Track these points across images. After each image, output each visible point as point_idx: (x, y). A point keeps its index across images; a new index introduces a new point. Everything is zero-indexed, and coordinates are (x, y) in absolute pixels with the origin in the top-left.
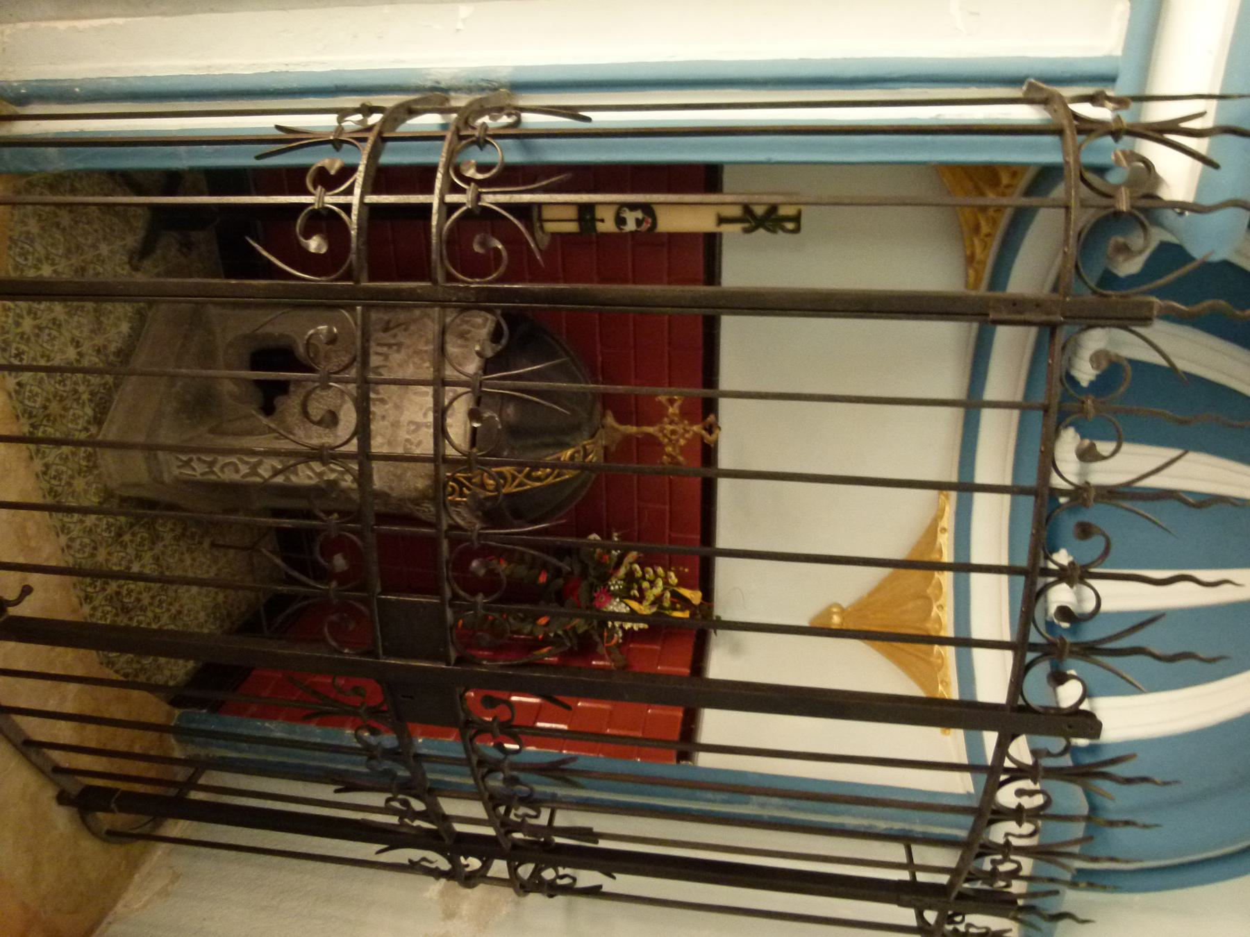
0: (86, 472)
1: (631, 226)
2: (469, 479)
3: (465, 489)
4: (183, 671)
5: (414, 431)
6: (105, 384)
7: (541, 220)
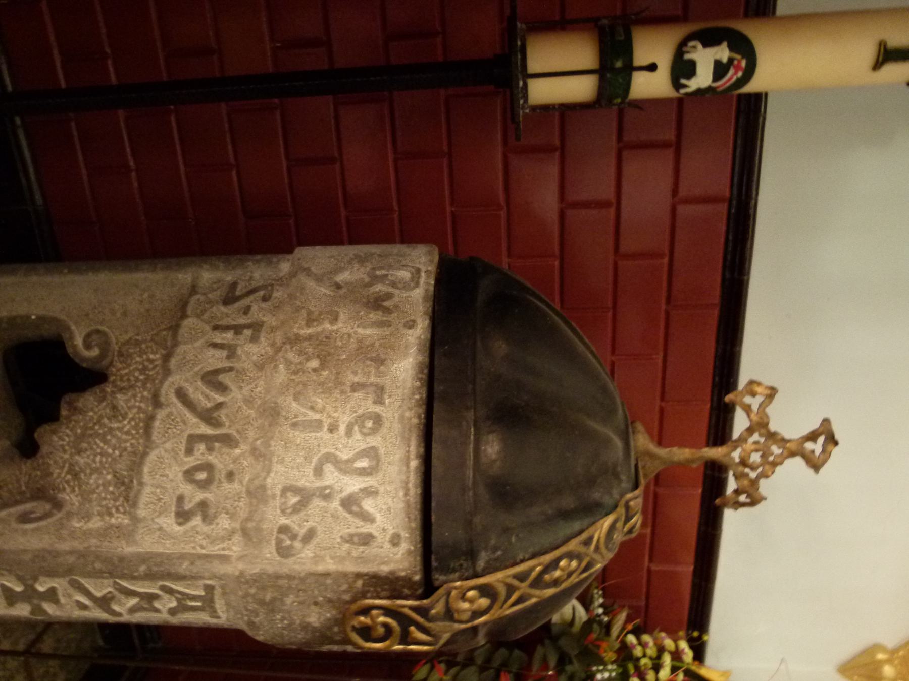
1: (703, 78)
2: (423, 612)
3: (412, 628)
5: (297, 509)
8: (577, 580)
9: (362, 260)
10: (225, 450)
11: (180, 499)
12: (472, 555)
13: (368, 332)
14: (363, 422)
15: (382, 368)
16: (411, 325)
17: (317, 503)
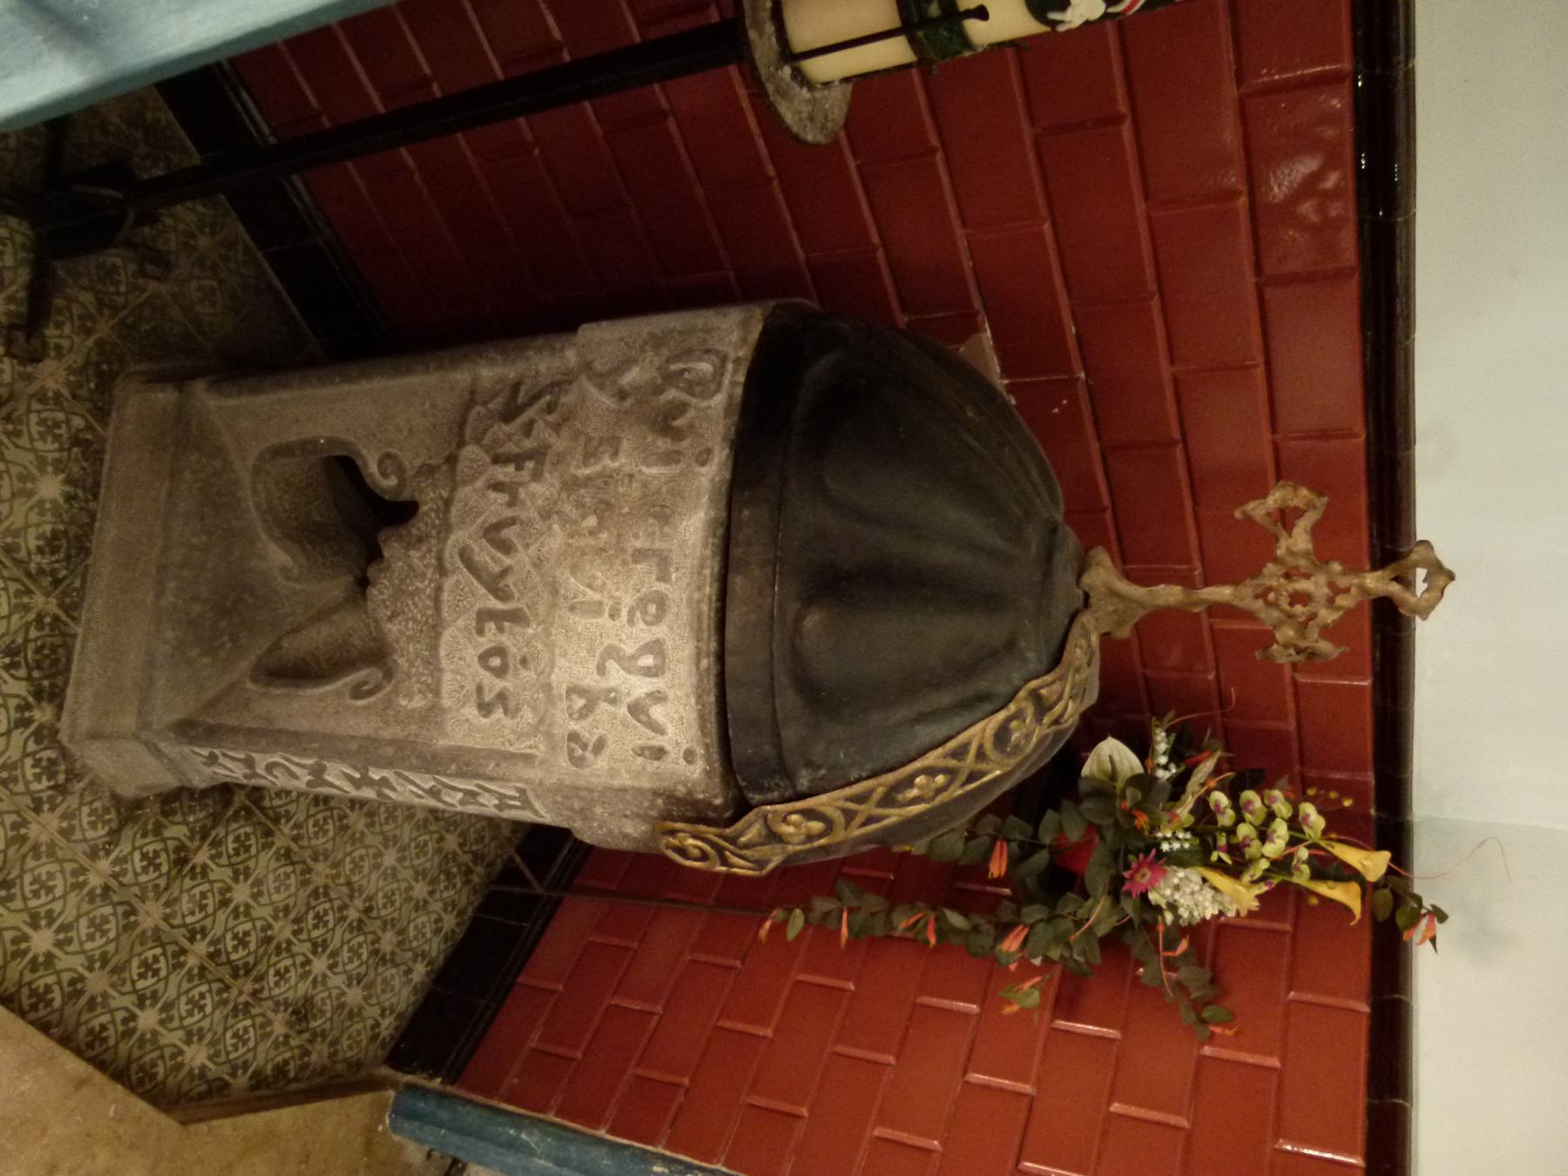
0: (51, 799)
4: (406, 992)
6: (39, 619)
7: (790, 56)
8: (960, 792)
9: (657, 342)
10: (517, 629)
11: (480, 689)
12: (788, 774)
13: (654, 471)
14: (645, 606)
15: (666, 529)
16: (704, 458)
17: (604, 706)
